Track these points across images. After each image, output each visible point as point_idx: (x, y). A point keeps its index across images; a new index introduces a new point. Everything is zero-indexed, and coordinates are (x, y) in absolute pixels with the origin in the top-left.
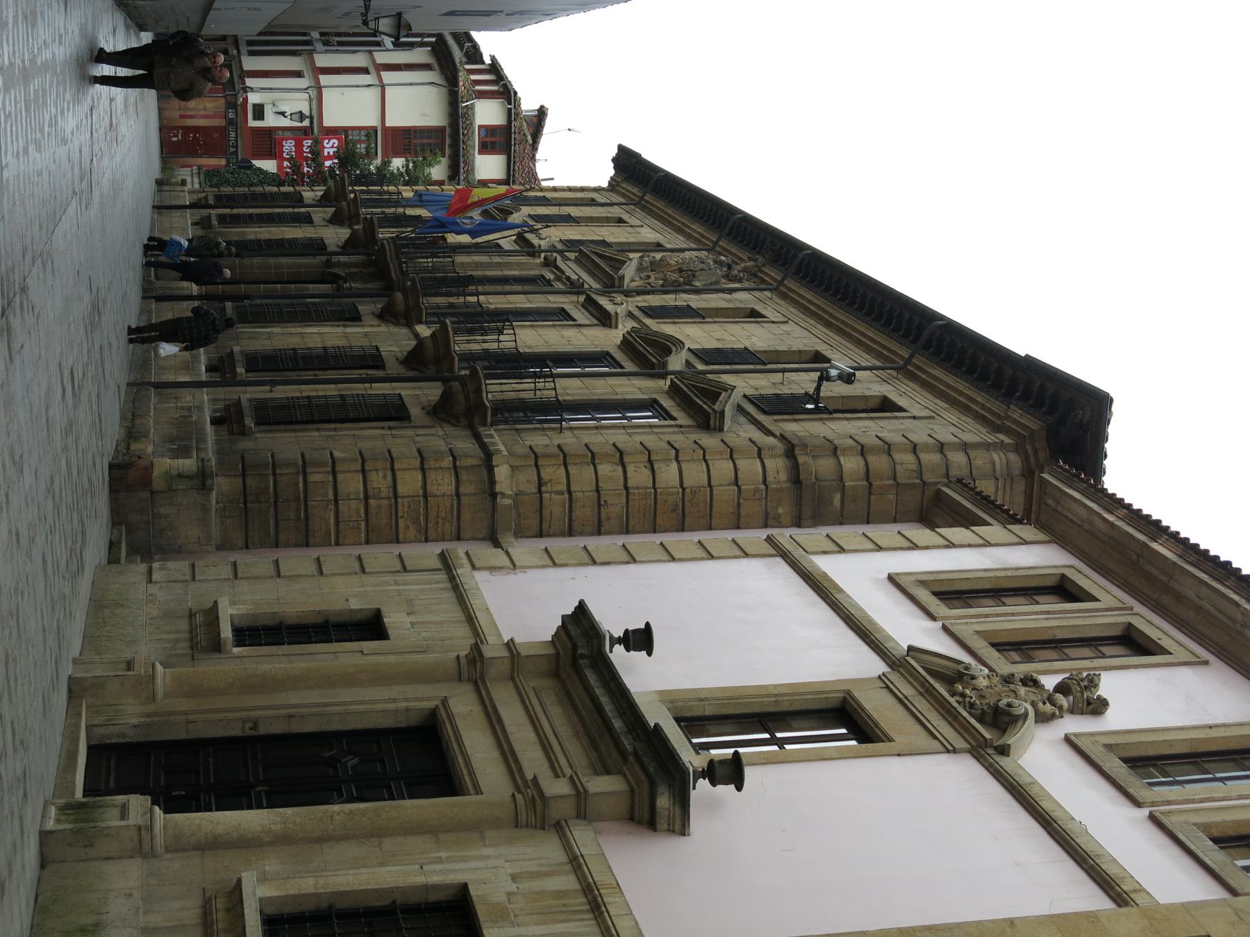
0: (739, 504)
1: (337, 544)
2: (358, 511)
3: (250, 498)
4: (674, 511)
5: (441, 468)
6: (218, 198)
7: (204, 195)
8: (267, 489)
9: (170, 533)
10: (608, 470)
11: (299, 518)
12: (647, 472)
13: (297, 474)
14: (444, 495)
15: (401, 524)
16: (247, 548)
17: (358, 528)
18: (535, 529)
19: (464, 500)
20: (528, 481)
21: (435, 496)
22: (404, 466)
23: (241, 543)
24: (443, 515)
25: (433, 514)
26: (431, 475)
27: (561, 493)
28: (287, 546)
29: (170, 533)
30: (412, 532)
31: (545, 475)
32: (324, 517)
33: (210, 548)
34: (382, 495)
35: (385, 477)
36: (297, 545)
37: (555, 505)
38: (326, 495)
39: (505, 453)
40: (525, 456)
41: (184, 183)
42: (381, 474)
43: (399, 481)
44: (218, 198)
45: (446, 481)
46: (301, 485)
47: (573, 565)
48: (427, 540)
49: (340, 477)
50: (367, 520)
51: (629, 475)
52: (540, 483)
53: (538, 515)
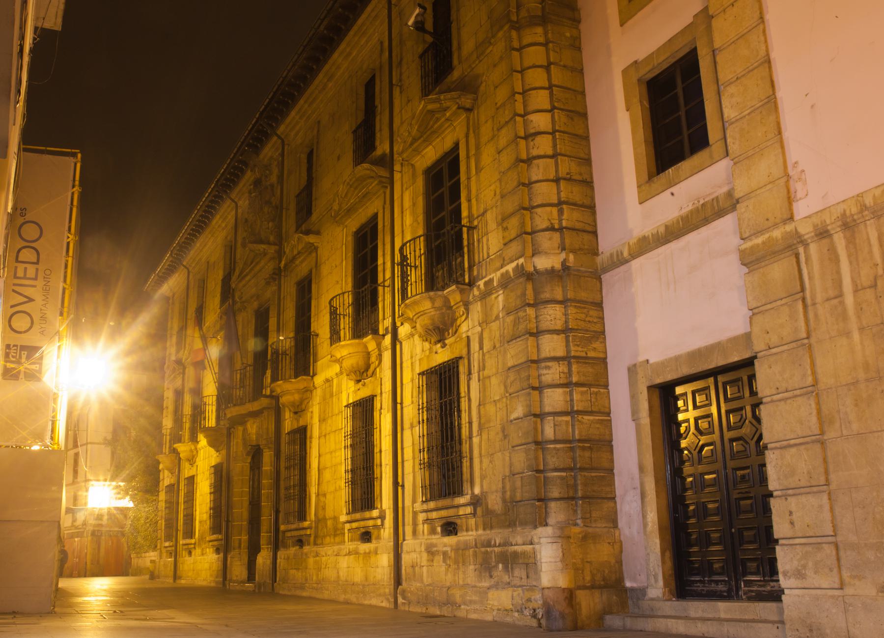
0: (565, 66)
1: (609, 414)
2: (582, 393)
3: (571, 494)
4: (572, 119)
5: (536, 317)
6: (168, 538)
7: (164, 550)
8: (562, 478)
9: (607, 572)
10: (538, 171)
11: (590, 448)
12: (539, 139)
13: (543, 449)
14: (566, 315)
15: (591, 354)
16: (614, 498)
17: (596, 394)
18: (587, 237)
19: (570, 295)
20: (550, 239)
21: (566, 322)
22: (535, 350)
23: (611, 504)
24: (583, 316)
25: (582, 325)
26: (544, 325)
27: (561, 212)
28: (612, 461)
29: (607, 572)
30: (597, 345)
31: (545, 225)
32: (587, 425)
33: (617, 534)
34: (566, 370)
35: (548, 368)
36: (611, 451)
37: (570, 217)
38: (567, 422)
39: (521, 261)
40: (524, 242)
41: (152, 562)
42: (545, 372)
43: (553, 354)
44: (168, 538)
45: (551, 312)
46: (558, 446)
47: (778, 117)
48: (603, 332)
49: (548, 409)
50: (590, 386)
51: (542, 153)
52: (551, 229)
53: (580, 233)
